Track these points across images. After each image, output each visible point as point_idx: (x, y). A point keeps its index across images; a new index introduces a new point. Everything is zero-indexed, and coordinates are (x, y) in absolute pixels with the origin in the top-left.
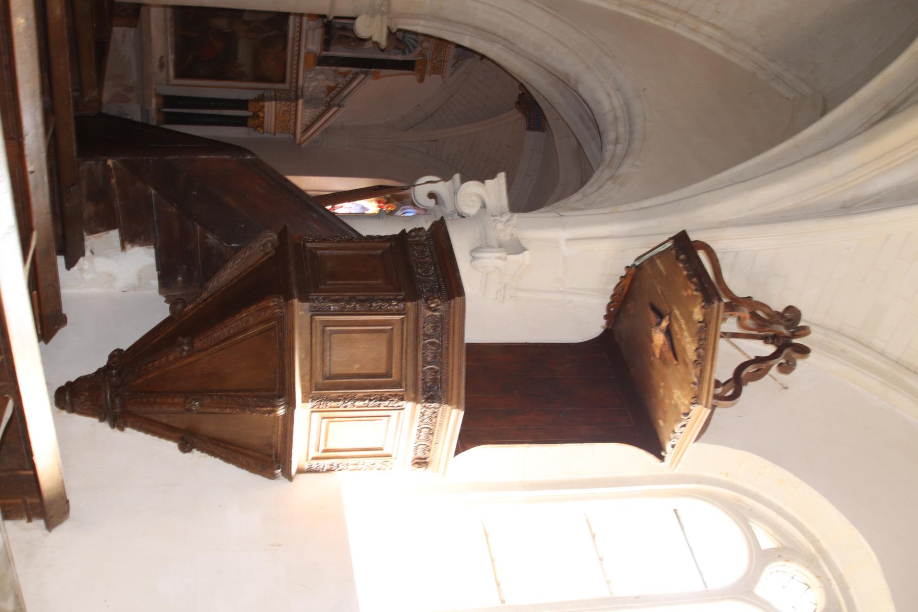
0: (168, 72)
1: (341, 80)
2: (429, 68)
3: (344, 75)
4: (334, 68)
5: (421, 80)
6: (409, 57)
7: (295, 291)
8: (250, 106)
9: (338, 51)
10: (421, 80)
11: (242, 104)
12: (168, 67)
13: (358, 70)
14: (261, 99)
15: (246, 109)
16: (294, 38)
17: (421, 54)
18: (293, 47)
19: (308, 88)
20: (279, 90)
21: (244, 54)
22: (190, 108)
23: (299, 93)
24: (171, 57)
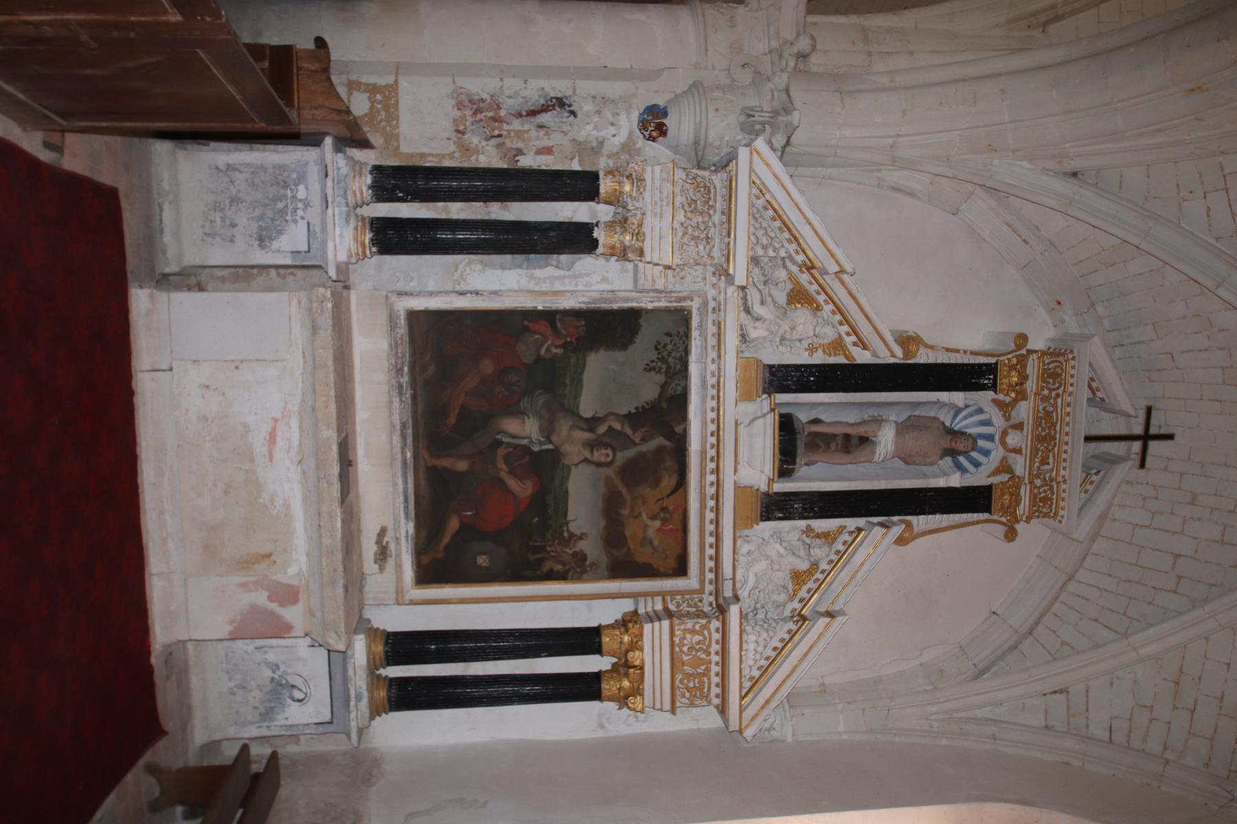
0: (399, 566)
1: (820, 552)
2: (1023, 508)
3: (828, 538)
4: (802, 524)
5: (1011, 535)
6: (977, 478)
7: (84, 154)
8: (606, 640)
9: (817, 477)
10: (1011, 535)
11: (584, 640)
12: (399, 556)
13: (861, 522)
14: (628, 622)
15: (597, 649)
16: (703, 453)
17: (1005, 467)
18: (703, 475)
19: (746, 581)
20: (672, 593)
21: (582, 508)
22: (277, 93)
23: (728, 593)
24: (408, 528)
